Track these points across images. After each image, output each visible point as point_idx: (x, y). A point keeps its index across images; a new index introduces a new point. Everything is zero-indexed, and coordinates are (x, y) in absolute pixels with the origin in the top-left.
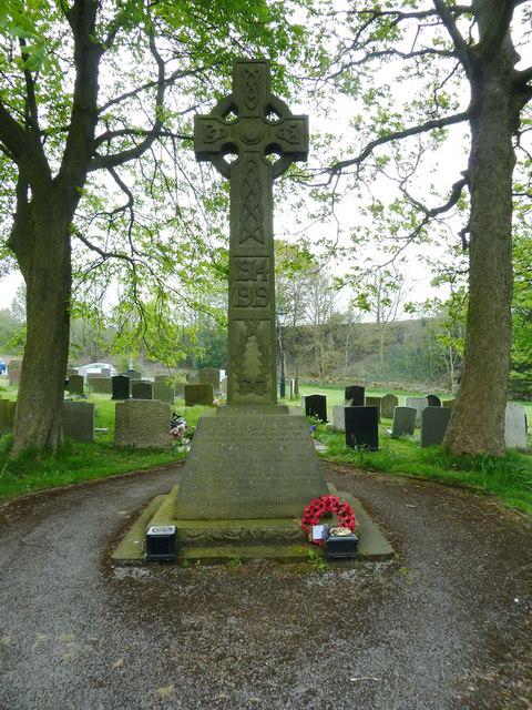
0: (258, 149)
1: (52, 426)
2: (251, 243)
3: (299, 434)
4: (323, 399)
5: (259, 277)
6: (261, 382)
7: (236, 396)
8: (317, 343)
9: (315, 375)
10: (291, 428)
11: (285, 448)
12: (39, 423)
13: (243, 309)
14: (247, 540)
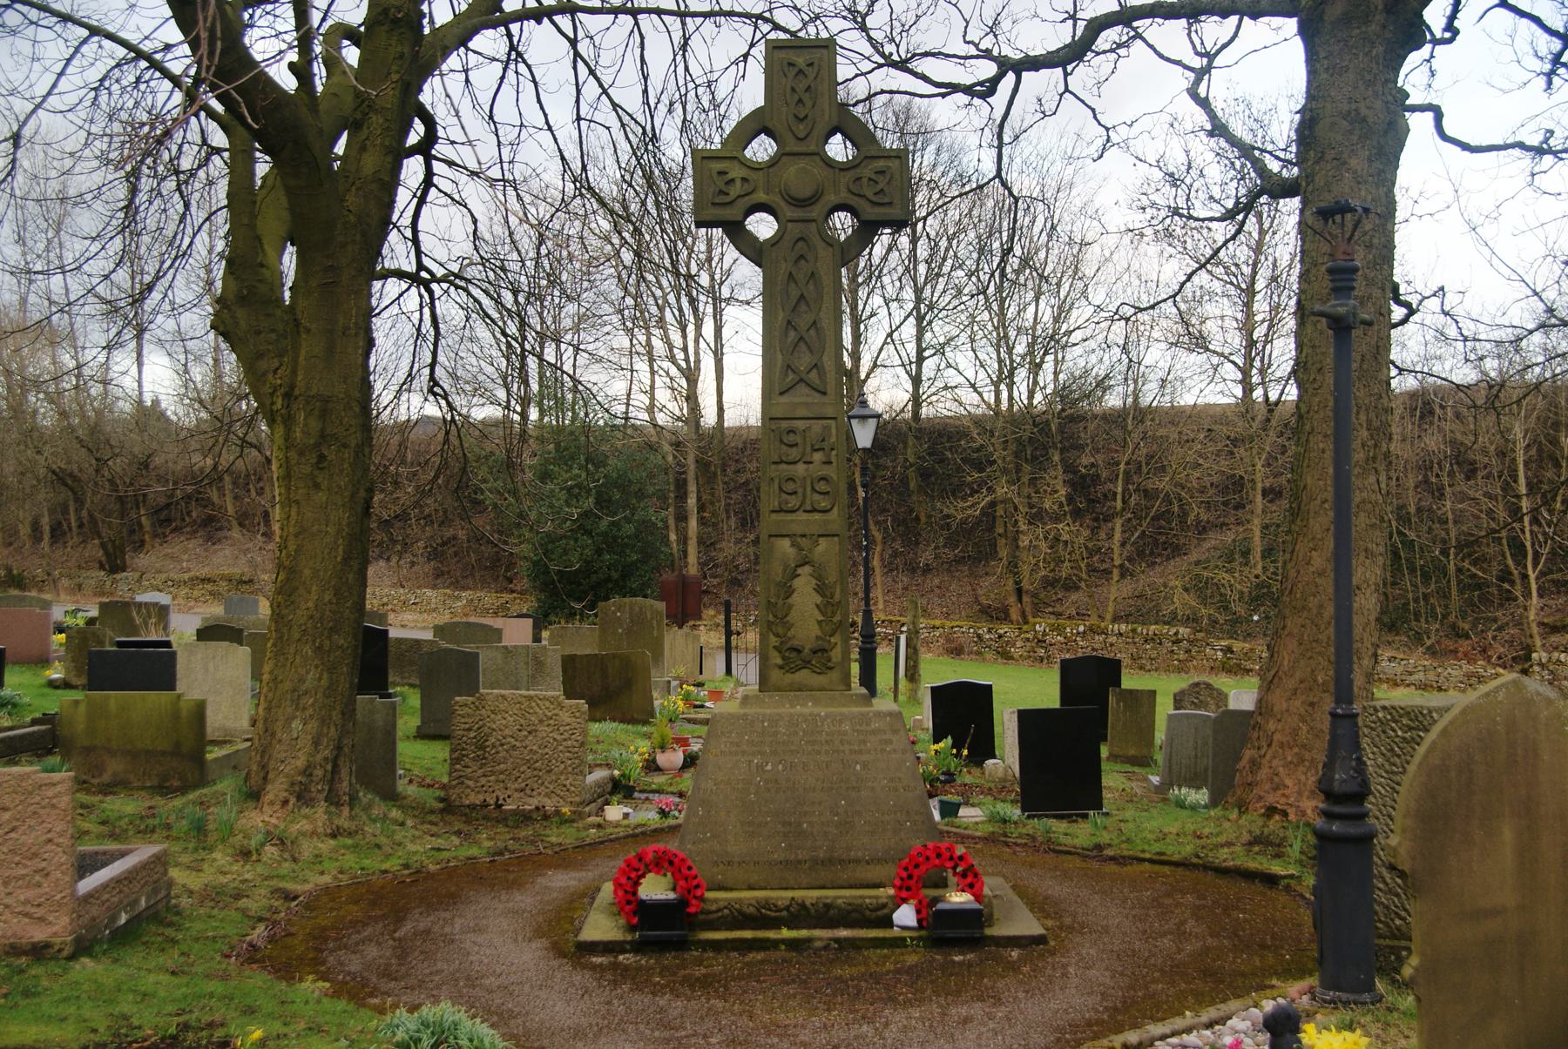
0: (814, 215)
1: (339, 748)
2: (802, 395)
3: (889, 742)
4: (982, 695)
5: (818, 457)
6: (821, 650)
7: (776, 676)
8: (1003, 490)
9: (998, 614)
10: (873, 732)
11: (865, 766)
12: (316, 743)
13: (790, 517)
14: (799, 915)
